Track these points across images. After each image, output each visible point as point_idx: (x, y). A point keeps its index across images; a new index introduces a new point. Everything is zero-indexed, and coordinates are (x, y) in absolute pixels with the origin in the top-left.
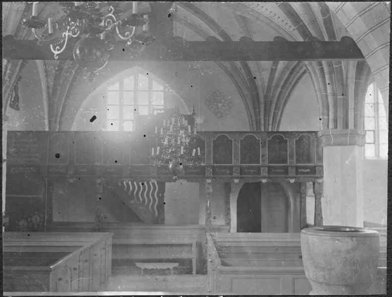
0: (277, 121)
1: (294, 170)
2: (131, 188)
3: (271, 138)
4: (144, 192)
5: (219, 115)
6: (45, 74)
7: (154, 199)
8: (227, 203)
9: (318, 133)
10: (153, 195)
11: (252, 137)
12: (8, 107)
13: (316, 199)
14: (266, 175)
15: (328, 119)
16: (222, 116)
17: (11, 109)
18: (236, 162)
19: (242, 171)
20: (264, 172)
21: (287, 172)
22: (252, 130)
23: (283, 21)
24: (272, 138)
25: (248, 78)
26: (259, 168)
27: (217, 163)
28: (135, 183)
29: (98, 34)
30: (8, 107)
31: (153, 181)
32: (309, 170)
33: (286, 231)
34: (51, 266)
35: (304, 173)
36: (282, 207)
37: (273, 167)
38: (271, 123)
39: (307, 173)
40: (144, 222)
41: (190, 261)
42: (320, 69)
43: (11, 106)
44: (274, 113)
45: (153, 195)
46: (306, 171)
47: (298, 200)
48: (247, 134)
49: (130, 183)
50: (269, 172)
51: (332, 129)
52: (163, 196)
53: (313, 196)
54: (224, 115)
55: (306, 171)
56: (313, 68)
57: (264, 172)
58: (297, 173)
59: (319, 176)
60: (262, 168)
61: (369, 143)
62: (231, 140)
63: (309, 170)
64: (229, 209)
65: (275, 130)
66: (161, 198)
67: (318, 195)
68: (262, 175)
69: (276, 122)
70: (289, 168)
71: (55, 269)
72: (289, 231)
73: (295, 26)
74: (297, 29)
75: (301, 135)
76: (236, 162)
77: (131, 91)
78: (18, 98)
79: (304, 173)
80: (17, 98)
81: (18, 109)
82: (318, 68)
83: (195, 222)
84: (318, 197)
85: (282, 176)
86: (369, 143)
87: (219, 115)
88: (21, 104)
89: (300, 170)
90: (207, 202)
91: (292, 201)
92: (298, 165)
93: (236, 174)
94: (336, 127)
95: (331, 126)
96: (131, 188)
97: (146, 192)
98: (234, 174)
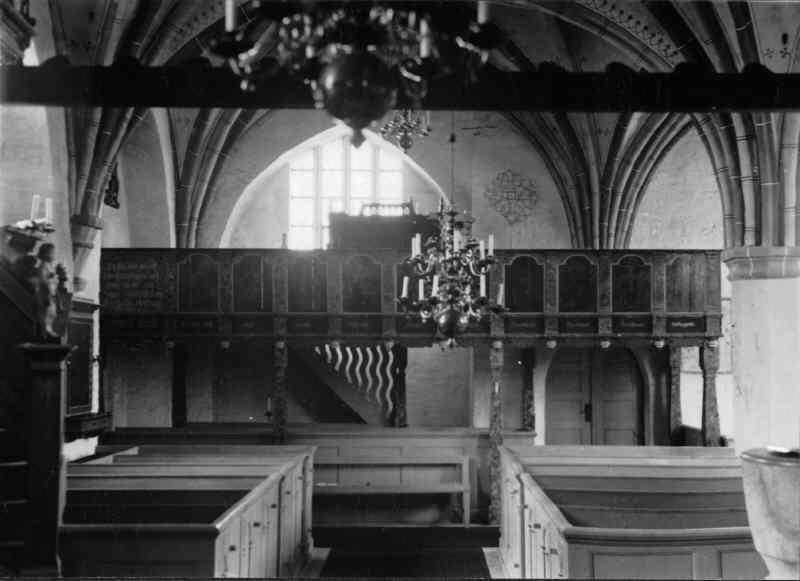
0: (625, 230)
2: (340, 357)
3: (619, 261)
4: (362, 364)
5: (511, 218)
6: (762, 486)
7: (386, 381)
8: (528, 385)
9: (722, 253)
10: (383, 371)
11: (582, 260)
12: (102, 205)
13: (705, 378)
14: (609, 332)
15: (743, 227)
16: (517, 220)
17: (108, 207)
18: (552, 309)
19: (562, 325)
20: (605, 329)
21: (649, 327)
22: (576, 247)
23: (622, 12)
24: (622, 262)
26: (594, 322)
28: (348, 349)
29: (310, 79)
30: (102, 205)
34: (217, 523)
36: (630, 395)
37: (624, 318)
38: (613, 231)
39: (689, 329)
40: (365, 423)
41: (460, 495)
42: (726, 130)
43: (107, 202)
44: (620, 213)
45: (383, 371)
46: (686, 325)
47: (664, 380)
51: (751, 246)
53: (698, 373)
54: (522, 218)
55: (686, 325)
56: (713, 128)
57: (605, 329)
58: (669, 329)
59: (712, 334)
62: (541, 267)
63: (691, 324)
64: (531, 398)
65: (621, 248)
66: (400, 380)
67: (707, 370)
68: (601, 333)
69: (623, 231)
71: (226, 526)
73: (678, 46)
74: (681, 51)
75: (676, 256)
76: (552, 309)
77: (688, 372)
78: (117, 183)
80: (114, 185)
81: (117, 206)
82: (723, 128)
83: (464, 420)
84: (708, 376)
85: (641, 334)
87: (511, 218)
88: (122, 196)
89: (675, 324)
90: (494, 385)
91: (651, 381)
92: (671, 314)
93: (550, 332)
94: (758, 243)
95: (750, 239)
96: (340, 357)
97: (360, 363)
98: (547, 331)
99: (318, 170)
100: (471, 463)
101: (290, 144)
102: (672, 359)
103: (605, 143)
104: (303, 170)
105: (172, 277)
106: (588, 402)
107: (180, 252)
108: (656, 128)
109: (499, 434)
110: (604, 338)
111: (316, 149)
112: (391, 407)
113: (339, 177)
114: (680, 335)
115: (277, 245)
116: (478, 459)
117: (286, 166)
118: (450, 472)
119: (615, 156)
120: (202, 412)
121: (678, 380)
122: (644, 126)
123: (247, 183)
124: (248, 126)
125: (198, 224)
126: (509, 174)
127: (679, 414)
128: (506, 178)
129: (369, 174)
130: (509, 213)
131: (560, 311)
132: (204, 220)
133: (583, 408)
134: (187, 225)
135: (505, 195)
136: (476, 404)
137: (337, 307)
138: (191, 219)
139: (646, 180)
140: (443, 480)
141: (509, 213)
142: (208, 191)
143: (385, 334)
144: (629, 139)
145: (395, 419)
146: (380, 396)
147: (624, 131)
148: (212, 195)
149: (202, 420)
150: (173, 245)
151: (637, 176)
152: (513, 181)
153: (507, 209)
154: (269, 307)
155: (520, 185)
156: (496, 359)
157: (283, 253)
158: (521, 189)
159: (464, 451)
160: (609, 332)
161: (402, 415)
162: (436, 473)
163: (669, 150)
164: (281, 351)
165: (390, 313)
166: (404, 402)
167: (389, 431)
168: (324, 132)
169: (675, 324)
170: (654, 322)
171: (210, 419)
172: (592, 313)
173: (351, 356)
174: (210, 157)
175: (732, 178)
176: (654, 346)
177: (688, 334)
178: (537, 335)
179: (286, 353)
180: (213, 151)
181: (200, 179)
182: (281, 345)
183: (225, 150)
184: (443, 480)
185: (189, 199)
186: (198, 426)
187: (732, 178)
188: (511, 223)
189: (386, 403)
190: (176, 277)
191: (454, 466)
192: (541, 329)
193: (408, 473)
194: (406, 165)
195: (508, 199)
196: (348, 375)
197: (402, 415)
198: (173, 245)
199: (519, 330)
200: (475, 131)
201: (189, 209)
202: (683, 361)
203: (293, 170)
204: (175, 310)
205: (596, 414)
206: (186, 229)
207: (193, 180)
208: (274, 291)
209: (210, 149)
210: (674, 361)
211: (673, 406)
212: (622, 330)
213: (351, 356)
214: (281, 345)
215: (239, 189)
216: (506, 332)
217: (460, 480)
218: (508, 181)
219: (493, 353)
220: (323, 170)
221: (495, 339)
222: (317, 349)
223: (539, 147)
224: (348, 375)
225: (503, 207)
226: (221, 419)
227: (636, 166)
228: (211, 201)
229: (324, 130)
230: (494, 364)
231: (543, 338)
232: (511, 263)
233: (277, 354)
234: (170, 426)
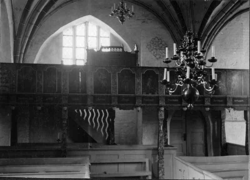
1: (116, 100)
4: (93, 118)
5: (158, 57)
14: (209, 104)
16: (160, 58)
25: (183, 28)
27: (97, 93)
28: (102, 111)
31: (91, 108)
32: (243, 101)
33: (206, 155)
35: (239, 103)
39: (241, 103)
40: (96, 142)
46: (240, 101)
48: (148, 69)
49: (93, 110)
50: (212, 102)
52: (113, 122)
54: (162, 57)
55: (240, 101)
58: (234, 103)
60: (206, 99)
61: (80, 60)
62: (135, 74)
66: (112, 124)
70: (113, 98)
72: (209, 155)
79: (239, 103)
86: (80, 60)
87: (158, 57)
89: (235, 101)
93: (185, 103)
98: (183, 103)
99: (75, 36)
100: (149, 161)
101: (64, 23)
102: (222, 116)
103: (198, 26)
104: (68, 36)
105: (14, 77)
106: (184, 133)
107: (17, 65)
108: (218, 22)
109: (162, 149)
110: (207, 107)
111: (74, 27)
112: (107, 135)
113: (83, 39)
114: (238, 105)
115: (60, 63)
116: (152, 159)
117: (61, 33)
118: (140, 166)
119: (201, 32)
120: (24, 139)
121: (224, 124)
122: (213, 20)
123: (45, 39)
124: (47, 14)
125: (24, 56)
126: (156, 39)
127: (225, 138)
128: (155, 40)
129: (72, 37)
130: (157, 54)
131: (118, 94)
132: (26, 55)
133: (183, 135)
134: (19, 55)
135: (155, 47)
136: (144, 134)
137: (90, 91)
138: (21, 53)
139: (211, 43)
140: (137, 170)
141: (157, 54)
142: (29, 41)
143: (113, 103)
144: (207, 25)
145: (110, 141)
146: (103, 131)
147: (207, 21)
148: (30, 44)
149: (24, 142)
150: (12, 62)
151: (208, 41)
152: (158, 42)
153: (156, 53)
154: (59, 91)
155: (161, 43)
156: (161, 115)
157: (61, 66)
158: (161, 45)
159: (146, 156)
160: (209, 104)
161: (113, 139)
162: (134, 167)
163: (221, 30)
164: (66, 111)
165: (162, 95)
166: (113, 134)
167: (106, 147)
168: (79, 19)
169: (215, 101)
170: (228, 100)
171: (28, 142)
172: (202, 96)
173: (103, 114)
174: (30, 27)
175: (209, 39)
176: (182, 110)
177: (241, 105)
178: (179, 105)
179: (67, 112)
180: (31, 24)
181: (25, 36)
182: (66, 108)
183: (37, 24)
184: (137, 170)
185: (20, 45)
186: (24, 145)
187: (209, 39)
188: (157, 59)
189: (105, 135)
190: (16, 77)
191: (141, 163)
192: (181, 102)
193: (122, 167)
194: (112, 34)
195: (156, 49)
196: (89, 121)
197: (113, 139)
198: (12, 62)
199: (147, 103)
200: (142, 21)
201: (20, 49)
202: (226, 116)
203: (64, 35)
204: (163, 94)
205: (189, 138)
206: (19, 57)
207: (22, 36)
208: (62, 84)
209: (30, 23)
210: (223, 117)
211: (222, 134)
212: (215, 103)
213: (103, 114)
214: (66, 108)
215: (42, 41)
216: (166, 103)
217: (144, 169)
218: (156, 42)
219: (160, 113)
220: (96, 37)
221: (161, 106)
222: (76, 111)
223: (168, 27)
224: (89, 121)
225: (154, 52)
226: (32, 142)
227: (208, 37)
228: (29, 46)
229: (79, 18)
230: (160, 117)
231: (158, 106)
232: (120, 72)
233: (63, 113)
234: (10, 145)
